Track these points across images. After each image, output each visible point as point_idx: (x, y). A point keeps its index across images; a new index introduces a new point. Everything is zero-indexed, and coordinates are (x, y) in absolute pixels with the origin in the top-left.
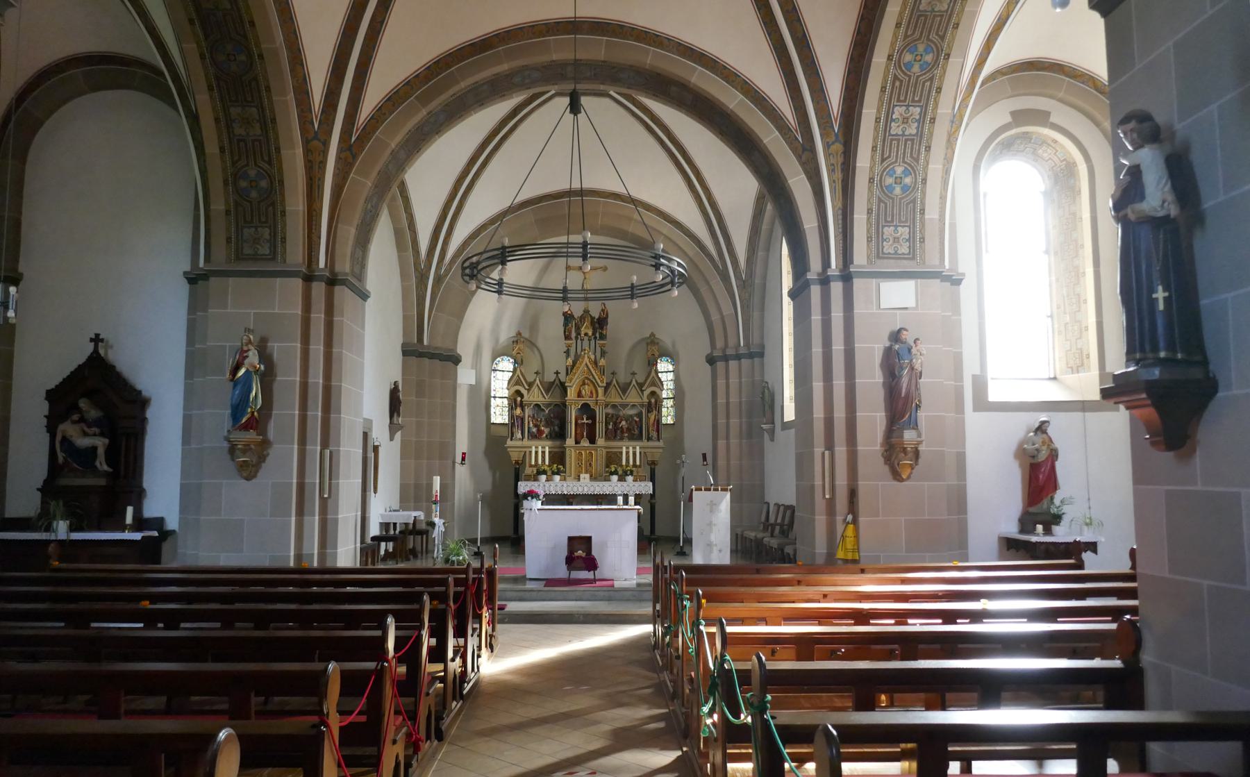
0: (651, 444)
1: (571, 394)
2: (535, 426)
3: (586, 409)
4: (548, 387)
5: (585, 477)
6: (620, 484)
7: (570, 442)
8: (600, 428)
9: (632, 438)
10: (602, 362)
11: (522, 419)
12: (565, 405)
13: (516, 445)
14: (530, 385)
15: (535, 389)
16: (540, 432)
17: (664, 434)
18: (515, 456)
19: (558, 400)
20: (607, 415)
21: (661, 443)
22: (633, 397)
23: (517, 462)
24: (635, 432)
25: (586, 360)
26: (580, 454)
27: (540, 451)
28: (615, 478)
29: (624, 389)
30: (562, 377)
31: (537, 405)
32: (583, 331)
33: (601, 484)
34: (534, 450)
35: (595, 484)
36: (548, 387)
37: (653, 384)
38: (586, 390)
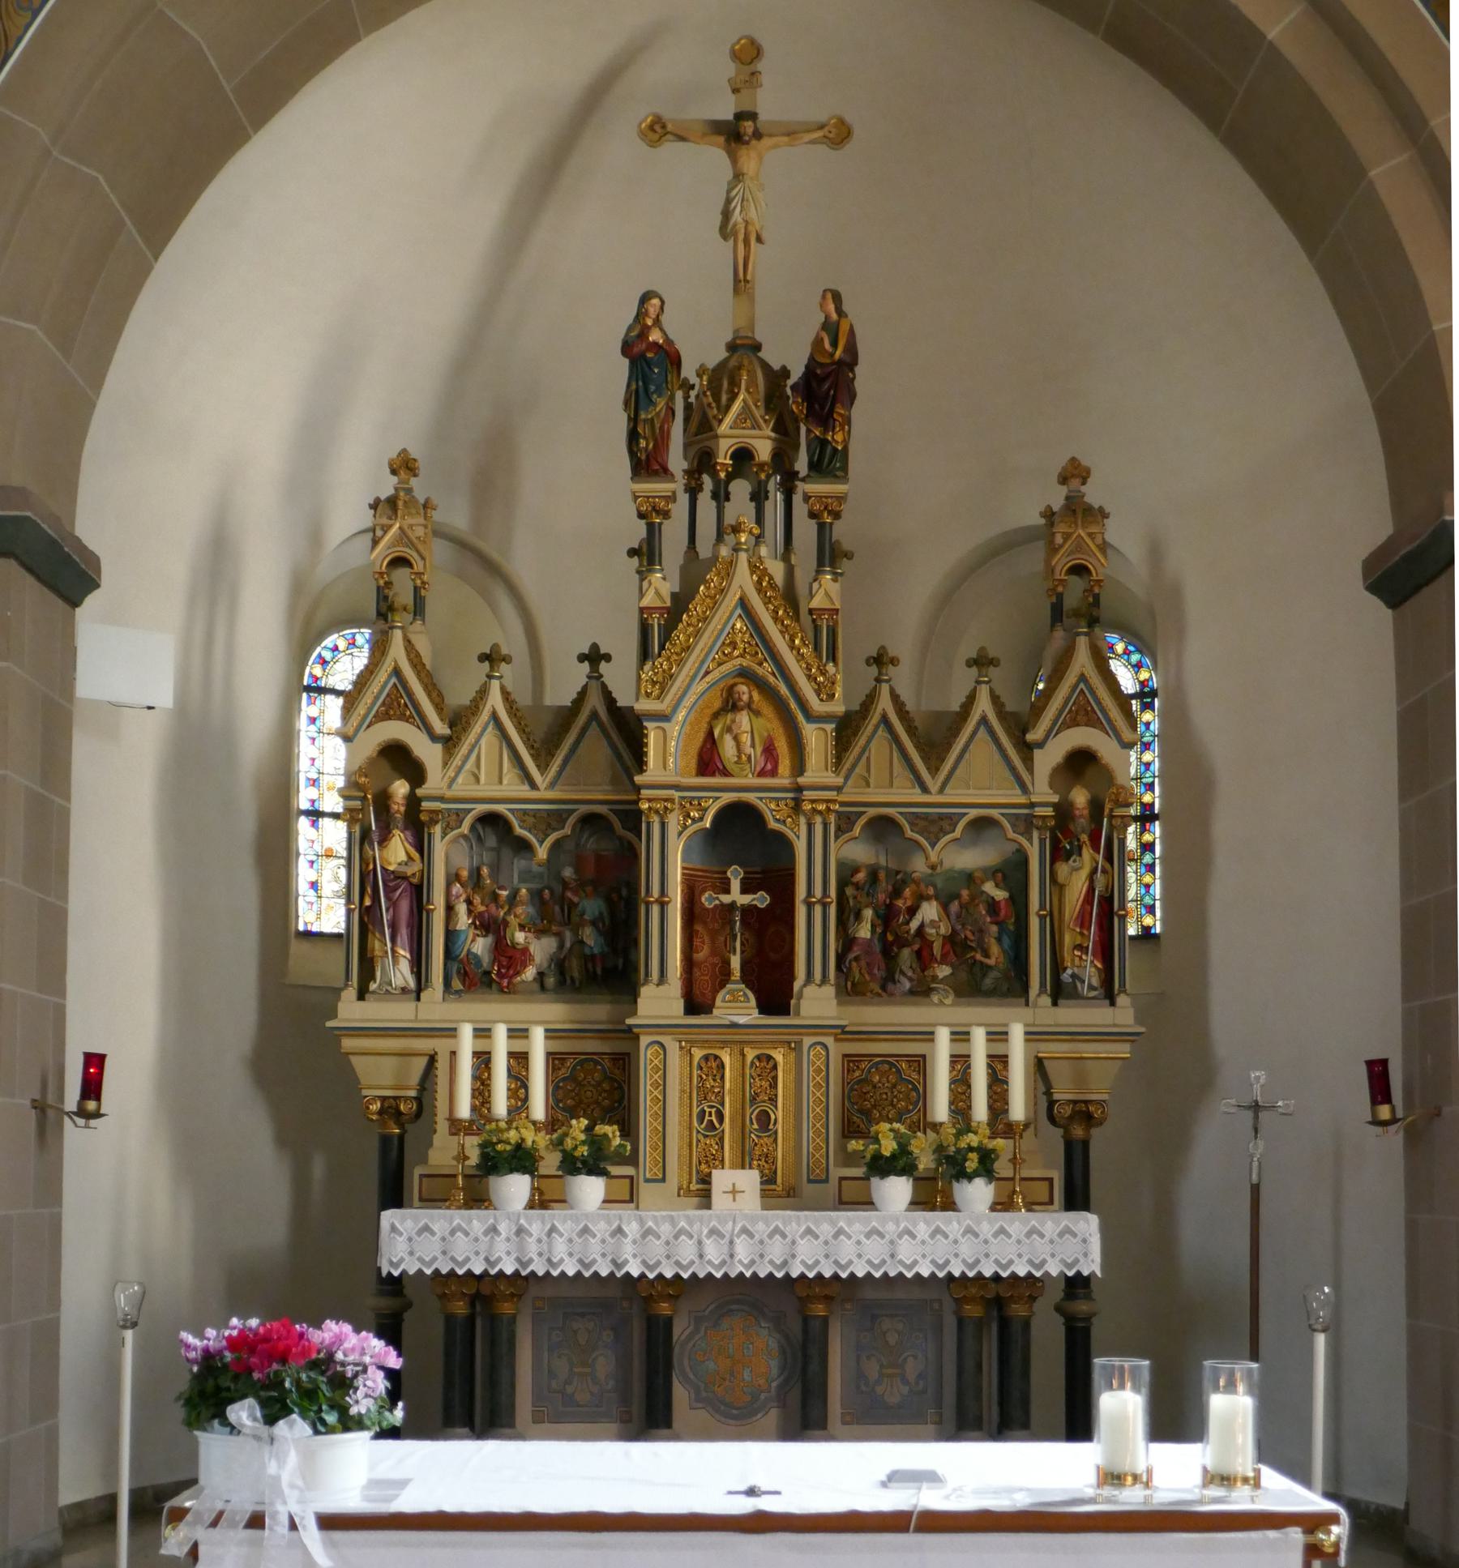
0: (1070, 1015)
1: (667, 755)
2: (487, 925)
3: (740, 833)
4: (548, 734)
5: (738, 1184)
6: (925, 1223)
7: (659, 1001)
8: (811, 935)
9: (973, 986)
10: (825, 592)
11: (419, 892)
12: (632, 818)
13: (389, 1021)
14: (460, 721)
15: (482, 741)
16: (509, 958)
17: (1131, 966)
18: (380, 1076)
19: (597, 794)
20: (847, 873)
21: (1122, 1015)
22: (978, 780)
23: (390, 1109)
24: (991, 957)
25: (743, 579)
26: (713, 1066)
27: (501, 1049)
28: (896, 1191)
29: (935, 739)
30: (622, 679)
31: (492, 821)
32: (726, 441)
33: (825, 1222)
34: (467, 1044)
35: (794, 1221)
36: (548, 734)
37: (1083, 713)
38: (745, 735)
